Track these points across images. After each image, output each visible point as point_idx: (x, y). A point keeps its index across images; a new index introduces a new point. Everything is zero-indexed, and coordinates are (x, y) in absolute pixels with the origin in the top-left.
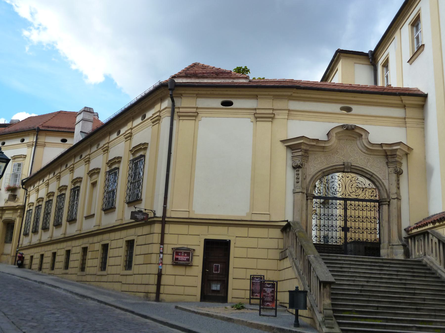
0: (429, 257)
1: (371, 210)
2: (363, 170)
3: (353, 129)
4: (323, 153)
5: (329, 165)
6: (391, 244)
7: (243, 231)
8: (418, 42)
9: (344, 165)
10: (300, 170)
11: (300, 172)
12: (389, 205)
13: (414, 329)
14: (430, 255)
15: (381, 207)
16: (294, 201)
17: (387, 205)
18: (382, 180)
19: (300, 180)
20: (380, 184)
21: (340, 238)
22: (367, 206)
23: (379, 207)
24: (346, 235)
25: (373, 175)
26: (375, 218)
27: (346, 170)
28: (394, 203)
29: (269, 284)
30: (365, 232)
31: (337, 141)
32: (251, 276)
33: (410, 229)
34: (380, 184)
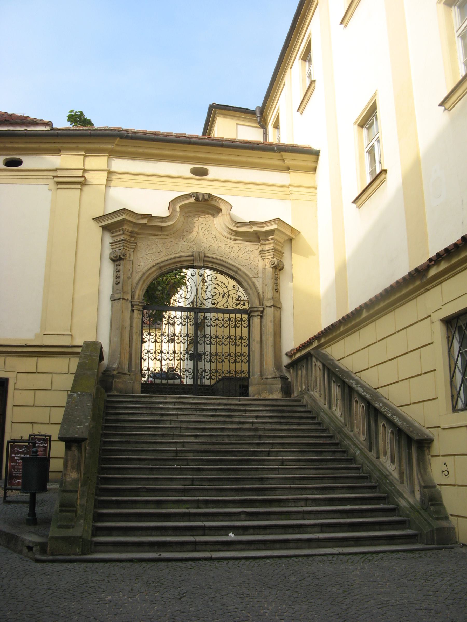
0: (312, 393)
1: (236, 326)
2: (222, 263)
3: (206, 200)
4: (160, 237)
5: (170, 257)
6: (264, 377)
7: (28, 364)
8: (310, 76)
9: (193, 256)
10: (122, 262)
11: (121, 268)
12: (262, 317)
13: (243, 517)
14: (313, 391)
15: (251, 320)
16: (112, 314)
17: (259, 317)
18: (253, 279)
19: (121, 280)
20: (248, 284)
21: (187, 370)
22: (229, 320)
23: (248, 321)
24: (196, 366)
25: (239, 272)
26: (241, 338)
27: (196, 264)
28: (269, 312)
29: (21, 447)
30: (226, 361)
31: (182, 219)
32: (30, 436)
33: (292, 352)
34: (248, 284)
